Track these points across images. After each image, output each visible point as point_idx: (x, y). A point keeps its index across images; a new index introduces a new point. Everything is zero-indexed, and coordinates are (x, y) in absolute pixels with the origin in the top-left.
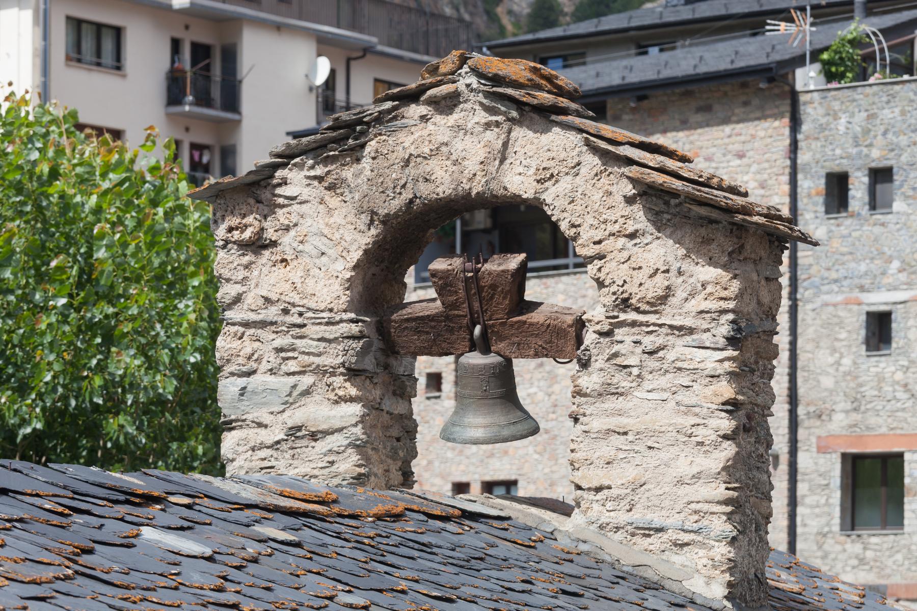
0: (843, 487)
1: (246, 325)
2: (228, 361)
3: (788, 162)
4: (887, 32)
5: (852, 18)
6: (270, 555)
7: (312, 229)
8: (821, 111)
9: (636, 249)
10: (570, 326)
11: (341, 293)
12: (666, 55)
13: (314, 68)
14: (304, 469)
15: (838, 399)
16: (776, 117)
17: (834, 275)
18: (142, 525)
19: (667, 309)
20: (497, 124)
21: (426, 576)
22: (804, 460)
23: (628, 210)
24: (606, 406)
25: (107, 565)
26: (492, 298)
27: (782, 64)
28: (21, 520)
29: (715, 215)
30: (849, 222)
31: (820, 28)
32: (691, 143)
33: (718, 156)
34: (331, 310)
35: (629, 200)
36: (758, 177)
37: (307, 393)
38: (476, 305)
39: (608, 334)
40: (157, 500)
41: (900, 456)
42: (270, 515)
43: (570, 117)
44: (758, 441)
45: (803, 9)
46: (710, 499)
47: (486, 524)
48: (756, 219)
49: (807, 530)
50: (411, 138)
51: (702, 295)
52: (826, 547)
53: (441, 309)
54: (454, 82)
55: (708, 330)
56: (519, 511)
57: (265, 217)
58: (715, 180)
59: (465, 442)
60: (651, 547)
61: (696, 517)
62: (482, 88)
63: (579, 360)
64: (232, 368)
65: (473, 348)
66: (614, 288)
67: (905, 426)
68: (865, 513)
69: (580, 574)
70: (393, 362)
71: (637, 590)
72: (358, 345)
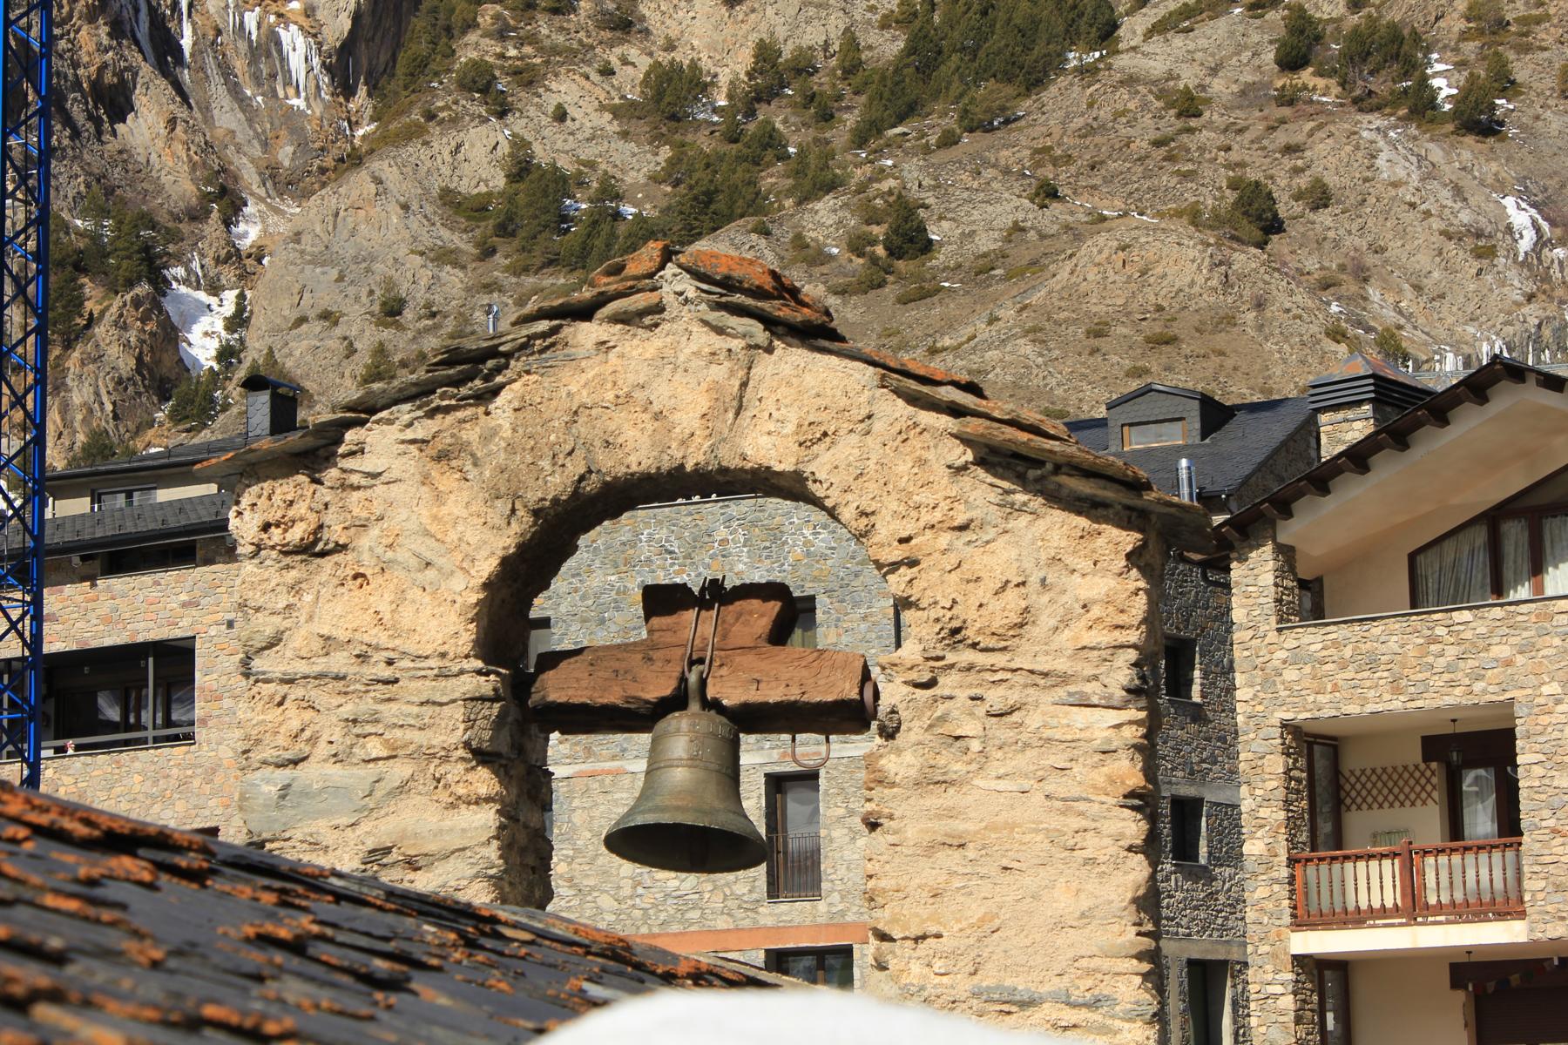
2: (258, 742)
9: (969, 549)
11: (461, 628)
19: (1025, 645)
34: (443, 655)
37: (403, 788)
51: (1083, 622)
54: (654, 289)
55: (1096, 678)
66: (933, 614)
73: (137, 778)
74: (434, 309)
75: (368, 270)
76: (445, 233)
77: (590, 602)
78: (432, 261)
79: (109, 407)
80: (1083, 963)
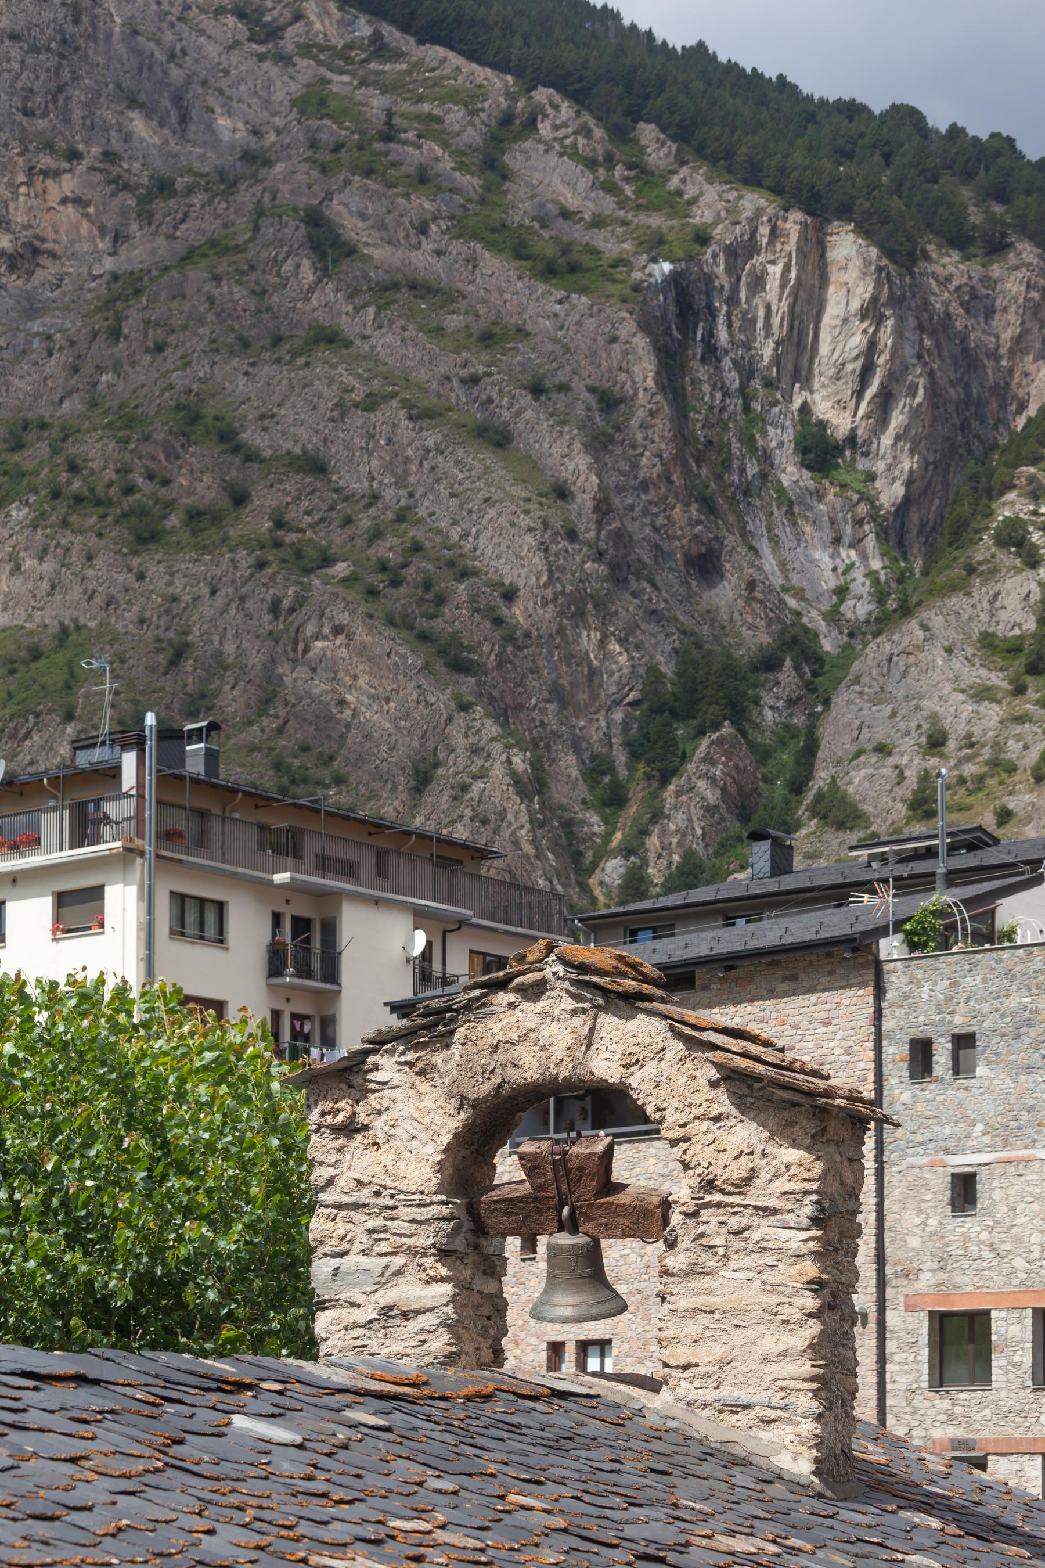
0: (931, 1345)
1: (339, 1207)
2: (322, 1242)
3: (873, 1029)
4: (968, 902)
5: (934, 889)
6: (360, 1441)
7: (403, 1113)
8: (904, 979)
9: (720, 1131)
10: (656, 1207)
11: (431, 1175)
12: (752, 926)
13: (411, 940)
14: (396, 1347)
15: (925, 1258)
16: (861, 985)
17: (919, 1138)
18: (233, 1413)
19: (752, 1190)
20: (584, 1011)
21: (515, 1458)
22: (892, 1318)
23: (712, 1094)
24: (693, 1285)
25: (197, 1455)
26: (579, 1180)
27: (865, 934)
28: (112, 1412)
29: (797, 1098)
30: (933, 1086)
31: (903, 899)
32: (778, 1011)
33: (804, 1024)
34: (422, 1192)
35: (713, 1085)
36: (844, 1043)
37: (399, 1273)
38: (564, 1187)
39: (694, 1215)
40: (249, 1387)
41: (987, 1313)
42: (361, 1400)
43: (655, 1004)
44: (843, 1318)
45: (885, 881)
46: (796, 1376)
47: (575, 1402)
48: (838, 1101)
49: (895, 1386)
50: (499, 1025)
51: (786, 1177)
52: (915, 1403)
53: (530, 1191)
54: (541, 970)
55: (792, 1211)
56: (608, 1388)
57: (357, 1102)
58: (798, 1064)
59: (555, 1321)
60: (739, 1424)
61: (783, 1394)
62: (569, 975)
63: (666, 1241)
64: (325, 1249)
65: (561, 1229)
66: (699, 1170)
67: (992, 1284)
68: (953, 1369)
69: (667, 1452)
70: (483, 1242)
71: (725, 1467)
72: (448, 1226)
73: (652, 1161)
74: (973, 739)
75: (917, 708)
76: (983, 672)
77: (1008, 1020)
78: (972, 697)
79: (699, 832)
80: (780, 1383)
